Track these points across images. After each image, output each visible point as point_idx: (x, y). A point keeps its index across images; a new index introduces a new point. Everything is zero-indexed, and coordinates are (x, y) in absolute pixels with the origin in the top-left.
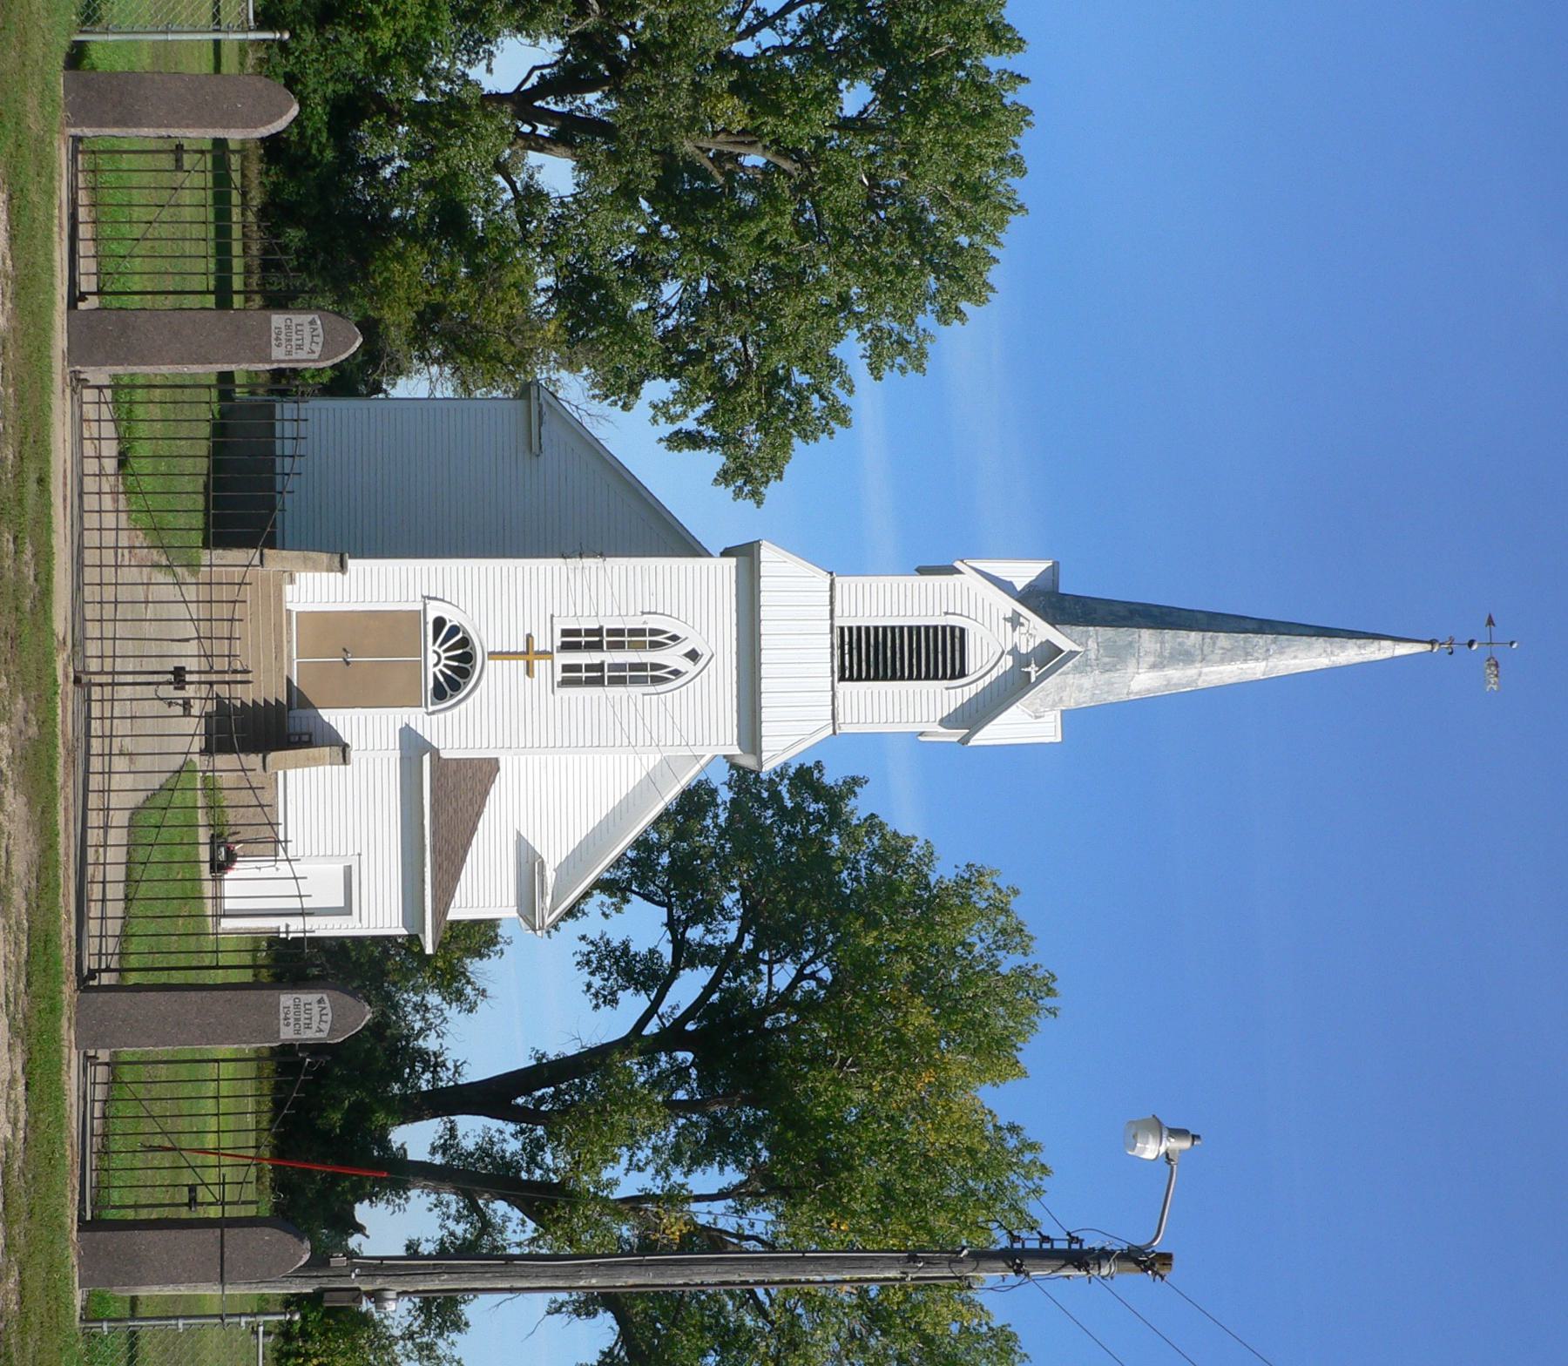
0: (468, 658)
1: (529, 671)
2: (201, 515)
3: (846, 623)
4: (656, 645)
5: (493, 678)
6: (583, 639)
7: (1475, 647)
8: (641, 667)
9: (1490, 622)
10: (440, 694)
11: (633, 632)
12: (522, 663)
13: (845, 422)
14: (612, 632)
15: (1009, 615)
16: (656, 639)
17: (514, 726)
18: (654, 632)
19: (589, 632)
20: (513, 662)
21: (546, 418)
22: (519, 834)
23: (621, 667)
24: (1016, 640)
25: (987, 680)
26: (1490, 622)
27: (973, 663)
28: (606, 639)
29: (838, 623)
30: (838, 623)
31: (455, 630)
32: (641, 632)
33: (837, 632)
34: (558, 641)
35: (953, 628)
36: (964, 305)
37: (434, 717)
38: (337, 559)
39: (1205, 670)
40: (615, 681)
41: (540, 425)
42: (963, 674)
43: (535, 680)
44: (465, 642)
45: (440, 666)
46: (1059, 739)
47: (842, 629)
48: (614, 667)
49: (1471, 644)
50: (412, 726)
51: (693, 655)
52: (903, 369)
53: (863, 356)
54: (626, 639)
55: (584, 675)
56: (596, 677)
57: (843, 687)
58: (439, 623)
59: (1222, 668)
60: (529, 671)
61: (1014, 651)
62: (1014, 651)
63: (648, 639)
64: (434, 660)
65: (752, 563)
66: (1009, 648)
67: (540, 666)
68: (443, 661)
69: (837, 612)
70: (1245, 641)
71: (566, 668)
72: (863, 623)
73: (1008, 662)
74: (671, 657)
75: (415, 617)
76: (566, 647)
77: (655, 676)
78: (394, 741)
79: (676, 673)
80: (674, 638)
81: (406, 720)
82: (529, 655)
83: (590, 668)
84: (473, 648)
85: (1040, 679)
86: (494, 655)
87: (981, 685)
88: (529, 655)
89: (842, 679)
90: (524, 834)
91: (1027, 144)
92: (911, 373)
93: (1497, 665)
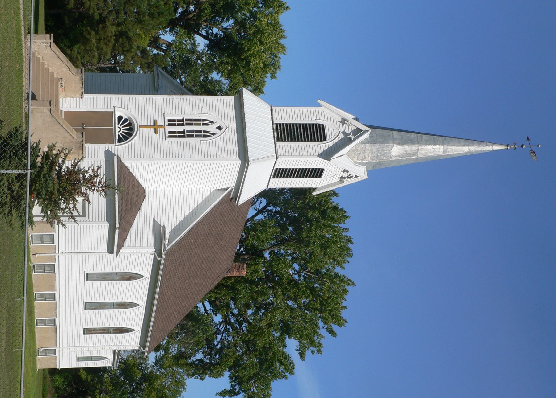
0: (132, 130)
1: (156, 132)
2: (37, 317)
3: (278, 122)
4: (204, 124)
5: (140, 135)
6: (177, 123)
7: (524, 147)
8: (200, 132)
9: (528, 139)
10: (120, 140)
11: (195, 120)
12: (153, 129)
13: (292, 373)
14: (187, 120)
15: (340, 120)
16: (204, 122)
17: (150, 150)
18: (203, 120)
19: (178, 121)
20: (149, 129)
21: (160, 77)
22: (154, 219)
23: (192, 132)
24: (344, 128)
25: (335, 141)
26: (528, 139)
27: (329, 134)
28: (185, 122)
29: (275, 122)
30: (275, 122)
31: (126, 120)
32: (199, 120)
33: (275, 125)
34: (167, 123)
35: (319, 125)
37: (119, 147)
38: (80, 71)
39: (420, 148)
40: (189, 136)
41: (158, 78)
42: (325, 140)
44: (130, 124)
45: (121, 132)
46: (366, 177)
47: (277, 124)
48: (188, 132)
49: (522, 146)
50: (110, 150)
51: (219, 128)
52: (313, 352)
53: (297, 350)
54: (193, 122)
55: (177, 135)
56: (182, 134)
57: (279, 143)
58: (120, 118)
59: (426, 147)
60: (156, 132)
61: (344, 132)
62: (344, 132)
63: (202, 122)
64: (118, 130)
65: (240, 95)
66: (342, 131)
67: (160, 130)
68: (122, 131)
69: (274, 118)
70: (434, 138)
71: (170, 132)
72: (285, 122)
73: (342, 136)
74: (211, 128)
75: (111, 114)
76: (169, 125)
77: (205, 135)
78: (103, 156)
79: (213, 134)
80: (212, 122)
81: (107, 148)
82: (155, 127)
83: (179, 132)
84: (134, 126)
85: (355, 140)
86: (142, 126)
87: (332, 143)
88: (155, 127)
89: (278, 140)
90: (156, 219)
92: (316, 354)
93: (534, 152)
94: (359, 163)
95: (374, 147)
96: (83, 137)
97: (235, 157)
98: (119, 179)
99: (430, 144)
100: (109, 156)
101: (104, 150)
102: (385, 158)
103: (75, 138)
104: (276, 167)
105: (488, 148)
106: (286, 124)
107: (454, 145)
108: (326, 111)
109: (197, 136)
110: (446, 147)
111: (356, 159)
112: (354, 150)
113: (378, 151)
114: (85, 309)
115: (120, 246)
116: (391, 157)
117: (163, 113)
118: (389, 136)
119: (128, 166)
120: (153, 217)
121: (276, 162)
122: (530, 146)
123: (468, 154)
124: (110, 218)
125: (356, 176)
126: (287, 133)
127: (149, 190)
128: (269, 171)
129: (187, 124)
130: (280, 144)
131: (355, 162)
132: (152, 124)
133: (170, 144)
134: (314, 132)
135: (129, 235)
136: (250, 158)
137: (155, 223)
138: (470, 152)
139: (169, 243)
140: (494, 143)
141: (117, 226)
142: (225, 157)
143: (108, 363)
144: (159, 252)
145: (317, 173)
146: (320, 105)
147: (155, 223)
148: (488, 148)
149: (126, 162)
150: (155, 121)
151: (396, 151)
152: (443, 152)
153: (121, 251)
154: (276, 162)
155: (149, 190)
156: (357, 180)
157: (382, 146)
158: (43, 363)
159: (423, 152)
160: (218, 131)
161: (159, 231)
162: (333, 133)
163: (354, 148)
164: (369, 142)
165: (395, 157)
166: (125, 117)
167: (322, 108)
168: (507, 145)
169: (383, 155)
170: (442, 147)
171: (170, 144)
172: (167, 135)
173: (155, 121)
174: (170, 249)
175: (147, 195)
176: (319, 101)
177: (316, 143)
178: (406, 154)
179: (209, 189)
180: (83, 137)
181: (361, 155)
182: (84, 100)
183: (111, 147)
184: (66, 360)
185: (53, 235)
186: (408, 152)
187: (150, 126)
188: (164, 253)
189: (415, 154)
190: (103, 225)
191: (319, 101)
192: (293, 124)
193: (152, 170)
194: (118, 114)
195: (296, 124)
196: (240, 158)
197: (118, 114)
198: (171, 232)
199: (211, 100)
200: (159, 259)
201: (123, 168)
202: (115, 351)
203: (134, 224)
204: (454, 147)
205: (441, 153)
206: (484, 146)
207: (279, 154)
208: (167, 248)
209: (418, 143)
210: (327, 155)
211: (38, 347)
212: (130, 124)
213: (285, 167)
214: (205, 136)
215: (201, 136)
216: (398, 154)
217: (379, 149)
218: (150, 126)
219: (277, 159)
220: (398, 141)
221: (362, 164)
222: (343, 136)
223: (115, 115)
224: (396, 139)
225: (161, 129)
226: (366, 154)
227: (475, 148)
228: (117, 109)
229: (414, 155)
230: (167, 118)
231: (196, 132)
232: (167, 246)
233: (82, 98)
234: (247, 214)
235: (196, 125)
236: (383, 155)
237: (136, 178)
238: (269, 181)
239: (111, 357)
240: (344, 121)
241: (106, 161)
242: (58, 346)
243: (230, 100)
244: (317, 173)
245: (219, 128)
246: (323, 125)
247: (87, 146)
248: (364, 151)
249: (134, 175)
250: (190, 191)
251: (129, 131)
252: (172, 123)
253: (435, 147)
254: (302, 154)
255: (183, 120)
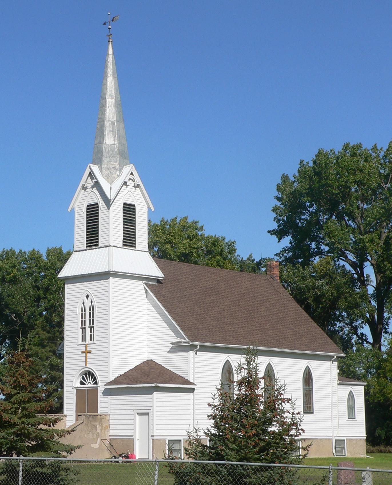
3: (85, 245)
4: (85, 311)
7: (110, 27)
8: (90, 313)
9: (105, 24)
10: (96, 383)
12: (88, 355)
14: (82, 326)
15: (84, 191)
16: (84, 310)
20: (88, 358)
22: (168, 352)
29: (85, 248)
30: (85, 248)
31: (83, 378)
35: (87, 209)
36: (287, 241)
39: (107, 120)
42: (97, 204)
43: (92, 350)
47: (87, 247)
48: (90, 324)
49: (110, 29)
51: (87, 297)
57: (100, 244)
58: (82, 383)
59: (107, 114)
61: (92, 188)
64: (89, 384)
66: (91, 189)
77: (92, 309)
79: (92, 302)
80: (83, 303)
81: (101, 394)
82: (86, 352)
85: (96, 179)
86: (86, 364)
88: (86, 352)
89: (97, 245)
91: (168, 218)
94: (120, 172)
95: (106, 160)
96: (81, 415)
97: (107, 283)
98: (121, 384)
99: (105, 111)
100: (108, 392)
101: (102, 396)
102: (116, 150)
103: (82, 421)
104: (121, 246)
105: (110, 58)
106: (87, 238)
107: (106, 89)
108: (77, 203)
109: (93, 317)
110: (107, 96)
111: (116, 176)
112: (108, 178)
113: (109, 157)
114: (313, 413)
115: (187, 382)
116: (115, 144)
117: (77, 346)
118: (97, 147)
119: (116, 376)
120: (166, 353)
121: (115, 247)
122: (109, 22)
123: (116, 76)
124: (149, 391)
125: (132, 174)
126: (93, 239)
127: (147, 356)
128: (128, 252)
129: (85, 325)
130: (100, 244)
131: (118, 176)
132: (84, 355)
133: (99, 339)
134: (92, 212)
135: (180, 374)
136: (107, 270)
137: (170, 351)
138: (113, 75)
139: (184, 339)
140: (107, 54)
141: (153, 385)
142: (107, 292)
143: (359, 392)
144: (192, 347)
145: (129, 210)
146: (73, 210)
147: (170, 351)
148: (110, 58)
149: (112, 378)
150: (83, 352)
151: (110, 140)
152: (112, 98)
153: (191, 381)
154: (115, 247)
155: (147, 356)
156: (135, 173)
157: (104, 154)
158: (361, 452)
159: (111, 116)
160: (89, 298)
161: (177, 348)
162: (95, 198)
163: (106, 178)
164: (101, 165)
165: (115, 141)
166: (81, 379)
167: (76, 206)
168: (109, 41)
169: (113, 152)
170: (108, 100)
171: (99, 339)
172: (92, 342)
173: (83, 352)
174: (188, 338)
175: (150, 359)
176: (69, 210)
177: (100, 212)
178: (112, 131)
179: (146, 304)
180: (81, 415)
181: (113, 171)
182: (68, 414)
183: (100, 391)
184: (358, 429)
185: (169, 440)
186: (111, 129)
187: (86, 357)
188: (191, 343)
189: (113, 123)
190: (155, 397)
191: (69, 210)
192: (87, 232)
193: (121, 355)
194: (78, 385)
195: (87, 229)
196: (108, 279)
197: (78, 385)
198: (178, 337)
199: (69, 305)
200: (198, 347)
201: (116, 381)
202: (339, 384)
203: (172, 370)
204: (108, 88)
205: (113, 100)
206: (108, 62)
207: (108, 244)
208: (188, 340)
209: (103, 121)
210: (108, 203)
211: (332, 456)
212: (86, 374)
213: (122, 238)
214: (93, 309)
215: (93, 313)
216: (112, 139)
217: (108, 155)
218: (86, 357)
219: (110, 246)
220: (102, 139)
221: (120, 170)
222: (95, 188)
223: (78, 388)
224: (100, 141)
225: (88, 348)
226: (111, 166)
227: (110, 70)
228: (74, 386)
229: (114, 124)
230: (80, 342)
231: (90, 317)
232: (185, 340)
233: (66, 416)
234: (59, 272)
235: (85, 318)
236: (113, 152)
237: (132, 368)
238: (79, 251)
239: (347, 389)
240: (84, 188)
241: (110, 395)
242: (331, 438)
243: (68, 288)
244: (129, 210)
245: (87, 297)
246: (88, 206)
247: (100, 412)
248: (108, 168)
249: (128, 370)
250: (148, 320)
251: (89, 374)
252: (83, 339)
253: (107, 105)
254: (112, 224)
255: (82, 329)
